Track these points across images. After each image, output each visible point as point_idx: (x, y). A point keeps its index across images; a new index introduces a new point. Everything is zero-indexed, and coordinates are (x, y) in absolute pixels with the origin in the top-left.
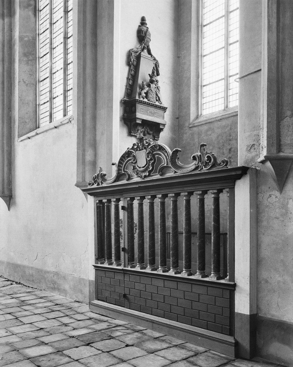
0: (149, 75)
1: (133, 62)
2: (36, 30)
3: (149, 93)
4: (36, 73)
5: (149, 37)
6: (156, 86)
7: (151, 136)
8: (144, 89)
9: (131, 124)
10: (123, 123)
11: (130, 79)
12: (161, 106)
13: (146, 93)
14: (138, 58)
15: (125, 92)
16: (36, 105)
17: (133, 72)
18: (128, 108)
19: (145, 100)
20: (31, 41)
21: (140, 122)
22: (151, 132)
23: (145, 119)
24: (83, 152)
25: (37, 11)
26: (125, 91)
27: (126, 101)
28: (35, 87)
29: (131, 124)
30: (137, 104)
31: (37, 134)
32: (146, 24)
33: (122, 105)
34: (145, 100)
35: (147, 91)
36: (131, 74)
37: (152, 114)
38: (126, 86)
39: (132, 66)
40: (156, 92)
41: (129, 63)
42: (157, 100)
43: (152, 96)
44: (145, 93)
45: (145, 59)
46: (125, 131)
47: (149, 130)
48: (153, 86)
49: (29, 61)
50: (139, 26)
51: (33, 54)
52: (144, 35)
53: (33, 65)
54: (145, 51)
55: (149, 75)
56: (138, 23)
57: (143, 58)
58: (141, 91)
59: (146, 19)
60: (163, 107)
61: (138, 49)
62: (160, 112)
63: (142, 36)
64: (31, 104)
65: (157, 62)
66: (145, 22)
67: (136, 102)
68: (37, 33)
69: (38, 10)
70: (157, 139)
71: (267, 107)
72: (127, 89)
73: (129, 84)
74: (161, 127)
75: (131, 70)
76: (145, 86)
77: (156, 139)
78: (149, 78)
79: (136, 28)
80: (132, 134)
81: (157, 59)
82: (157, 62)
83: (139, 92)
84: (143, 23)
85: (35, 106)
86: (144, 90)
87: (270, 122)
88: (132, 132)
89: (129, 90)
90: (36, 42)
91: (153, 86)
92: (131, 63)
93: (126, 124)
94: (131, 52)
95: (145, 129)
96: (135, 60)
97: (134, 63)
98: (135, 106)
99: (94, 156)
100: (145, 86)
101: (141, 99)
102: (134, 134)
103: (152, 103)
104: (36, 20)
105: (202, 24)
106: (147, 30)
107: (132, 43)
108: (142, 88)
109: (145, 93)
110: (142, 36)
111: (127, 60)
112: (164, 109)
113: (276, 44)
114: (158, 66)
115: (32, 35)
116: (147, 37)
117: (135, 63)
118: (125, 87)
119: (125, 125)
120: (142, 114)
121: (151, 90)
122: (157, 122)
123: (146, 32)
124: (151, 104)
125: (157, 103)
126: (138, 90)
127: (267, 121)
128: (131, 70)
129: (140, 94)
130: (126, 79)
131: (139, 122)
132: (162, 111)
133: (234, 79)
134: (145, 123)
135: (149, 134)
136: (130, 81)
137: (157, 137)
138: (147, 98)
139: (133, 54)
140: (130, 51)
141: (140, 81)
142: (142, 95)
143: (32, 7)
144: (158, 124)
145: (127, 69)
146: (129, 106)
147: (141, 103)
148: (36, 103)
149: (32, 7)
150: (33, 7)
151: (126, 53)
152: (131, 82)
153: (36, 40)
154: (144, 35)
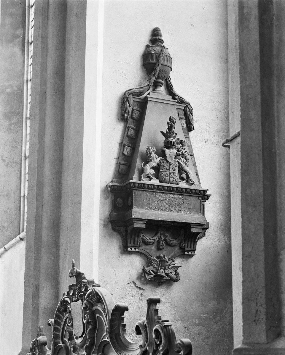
0: (162, 132)
1: (132, 112)
2: (23, 74)
3: (161, 168)
4: (22, 144)
5: (166, 63)
6: (178, 151)
7: (177, 249)
8: (151, 161)
9: (126, 231)
10: (110, 230)
11: (124, 146)
12: (191, 190)
13: (157, 169)
14: (143, 104)
15: (115, 170)
16: (20, 197)
17: (131, 132)
18: (120, 200)
19: (155, 182)
20: (16, 92)
21: (144, 226)
22: (175, 242)
23: (153, 218)
24: (35, 290)
25: (26, 44)
26: (116, 168)
27: (115, 187)
28: (19, 166)
29: (126, 231)
30: (134, 191)
31: (6, 250)
32: (162, 42)
33: (108, 196)
34: (155, 182)
35: (158, 164)
36: (128, 136)
37: (174, 207)
38: (118, 158)
39: (130, 120)
40: (178, 162)
41: (122, 117)
42: (182, 179)
43: (171, 173)
44: (153, 168)
45: (159, 104)
46: (115, 245)
47: (169, 239)
48: (171, 153)
49: (11, 125)
50: (148, 46)
51: (18, 114)
52: (155, 61)
53: (17, 132)
54: (162, 89)
55: (162, 132)
56: (145, 39)
57: (153, 103)
58: (144, 165)
59: (162, 31)
60: (195, 190)
61: (141, 88)
62: (193, 201)
63: (154, 63)
64: (12, 196)
65: (188, 105)
66: (160, 38)
67: (131, 187)
68: (25, 79)
69: (28, 43)
70: (190, 253)
71: (242, 217)
72: (118, 164)
73: (123, 154)
74: (194, 230)
75: (129, 128)
76: (154, 155)
77: (186, 253)
78: (164, 139)
79: (141, 49)
80: (129, 249)
81: (187, 99)
82: (187, 106)
83: (140, 167)
84: (154, 39)
85: (18, 198)
86: (151, 163)
87: (249, 256)
88: (129, 245)
89: (122, 166)
90: (23, 93)
91: (171, 153)
92: (126, 115)
93: (116, 232)
94: (127, 96)
95: (161, 237)
96: (135, 108)
97: (134, 115)
98: (130, 195)
99: (53, 298)
100: (154, 155)
101: (145, 181)
102: (133, 249)
103: (169, 185)
104: (24, 59)
105: (29, 41)
106: (162, 50)
107: (132, 77)
108: (146, 159)
109: (153, 168)
110: (154, 63)
111: (120, 111)
112: (203, 196)
113: (258, 57)
114: (189, 113)
115: (18, 83)
116: (162, 62)
117: (136, 114)
118: (115, 160)
119: (115, 233)
120: (143, 211)
121: (168, 161)
122: (184, 221)
123: (159, 55)
124: (168, 187)
125: (183, 185)
126: (139, 163)
127: (243, 254)
128: (129, 128)
129: (142, 171)
130: (117, 145)
131: (137, 225)
132: (196, 198)
133: (222, 144)
134: (154, 226)
135: (171, 245)
136: (125, 149)
137: (189, 249)
138: (157, 178)
139: (131, 99)
140: (125, 94)
141: (143, 147)
142: (147, 173)
143: (19, 40)
144: (186, 226)
145: (120, 127)
146: (121, 195)
147: (145, 188)
148: (20, 194)
149: (19, 40)
150: (20, 39)
151: (118, 98)
152: (127, 151)
153: (23, 90)
154: (155, 61)
